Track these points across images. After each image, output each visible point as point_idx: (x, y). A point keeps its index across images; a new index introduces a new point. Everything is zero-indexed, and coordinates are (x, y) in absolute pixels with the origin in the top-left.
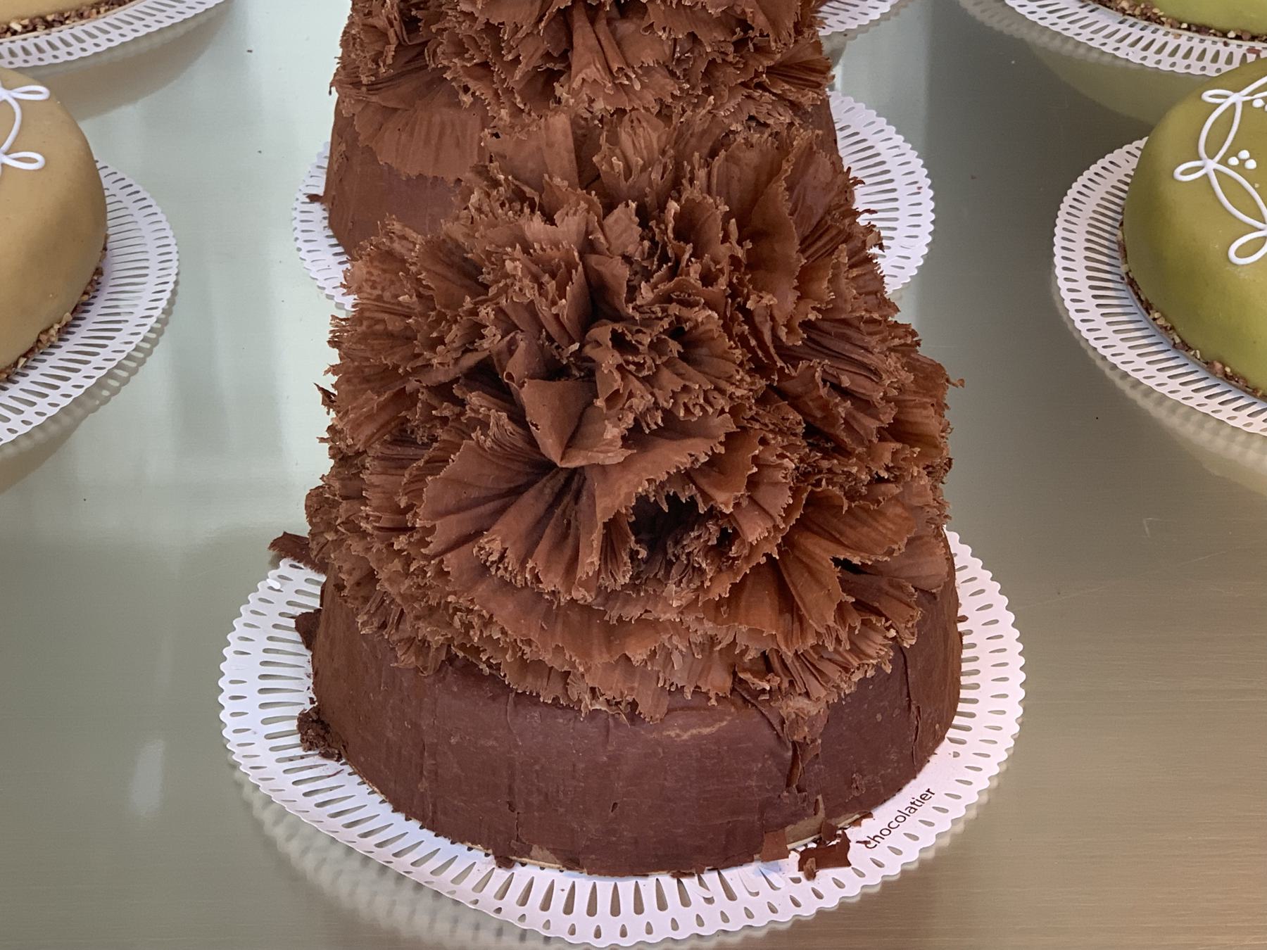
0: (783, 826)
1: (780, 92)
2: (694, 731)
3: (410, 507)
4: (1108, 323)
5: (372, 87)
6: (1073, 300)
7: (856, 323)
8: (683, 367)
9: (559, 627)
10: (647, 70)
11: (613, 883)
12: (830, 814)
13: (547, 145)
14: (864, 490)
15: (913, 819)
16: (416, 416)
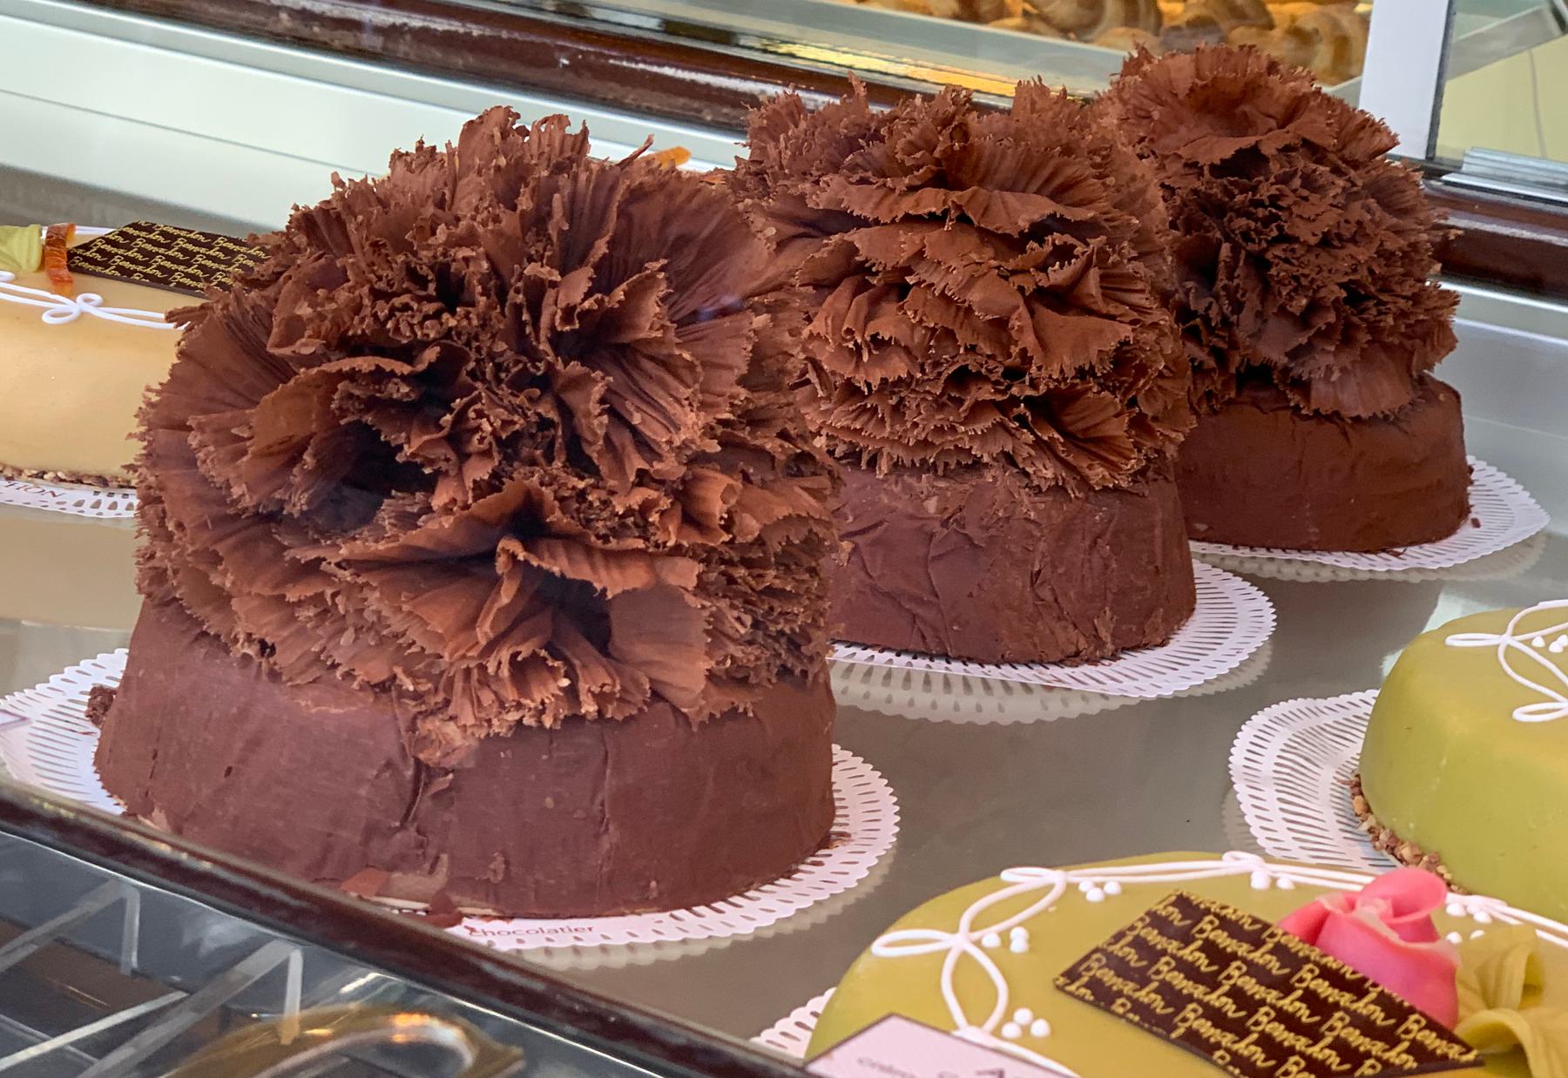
12: (454, 883)
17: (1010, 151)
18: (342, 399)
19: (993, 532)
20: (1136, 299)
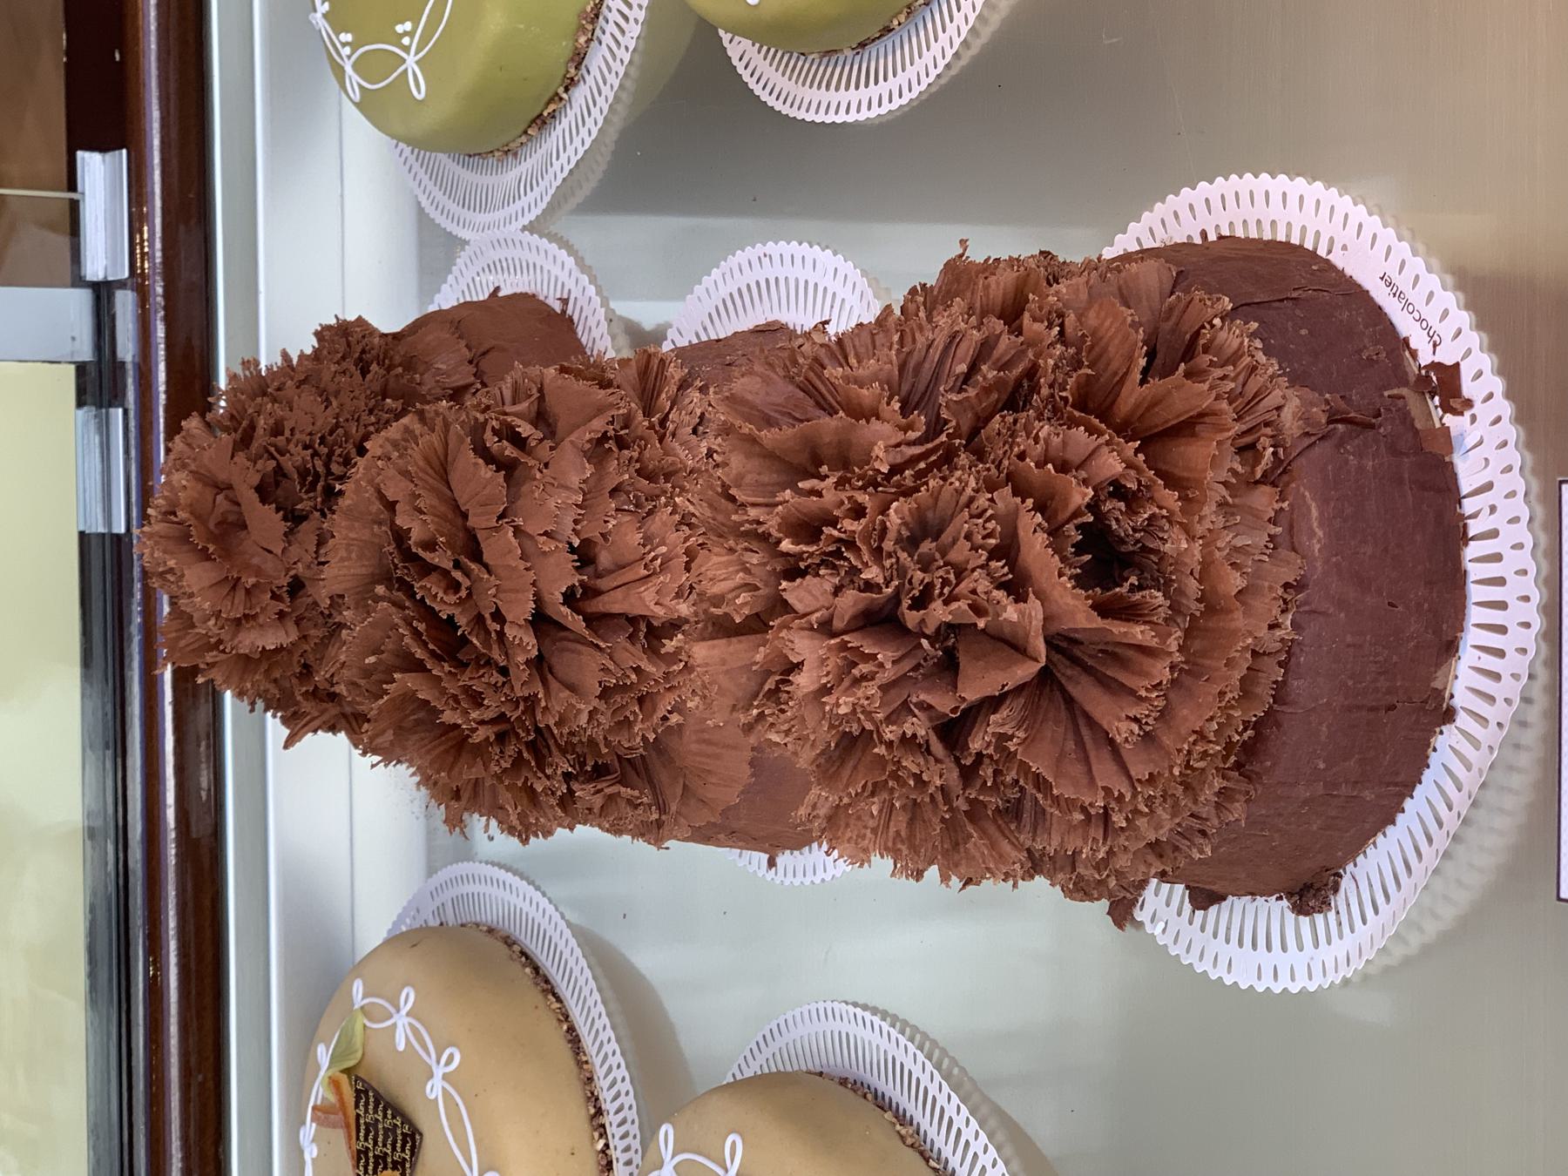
0: (1416, 432)
1: (669, 403)
2: (1315, 524)
3: (1084, 810)
4: (903, 70)
5: (662, 810)
6: (880, 105)
7: (903, 356)
8: (946, 537)
9: (1207, 662)
10: (647, 540)
11: (1474, 606)
12: (1404, 382)
13: (724, 665)
14: (1072, 351)
15: (1411, 295)
16: (993, 801)
17: (428, 502)
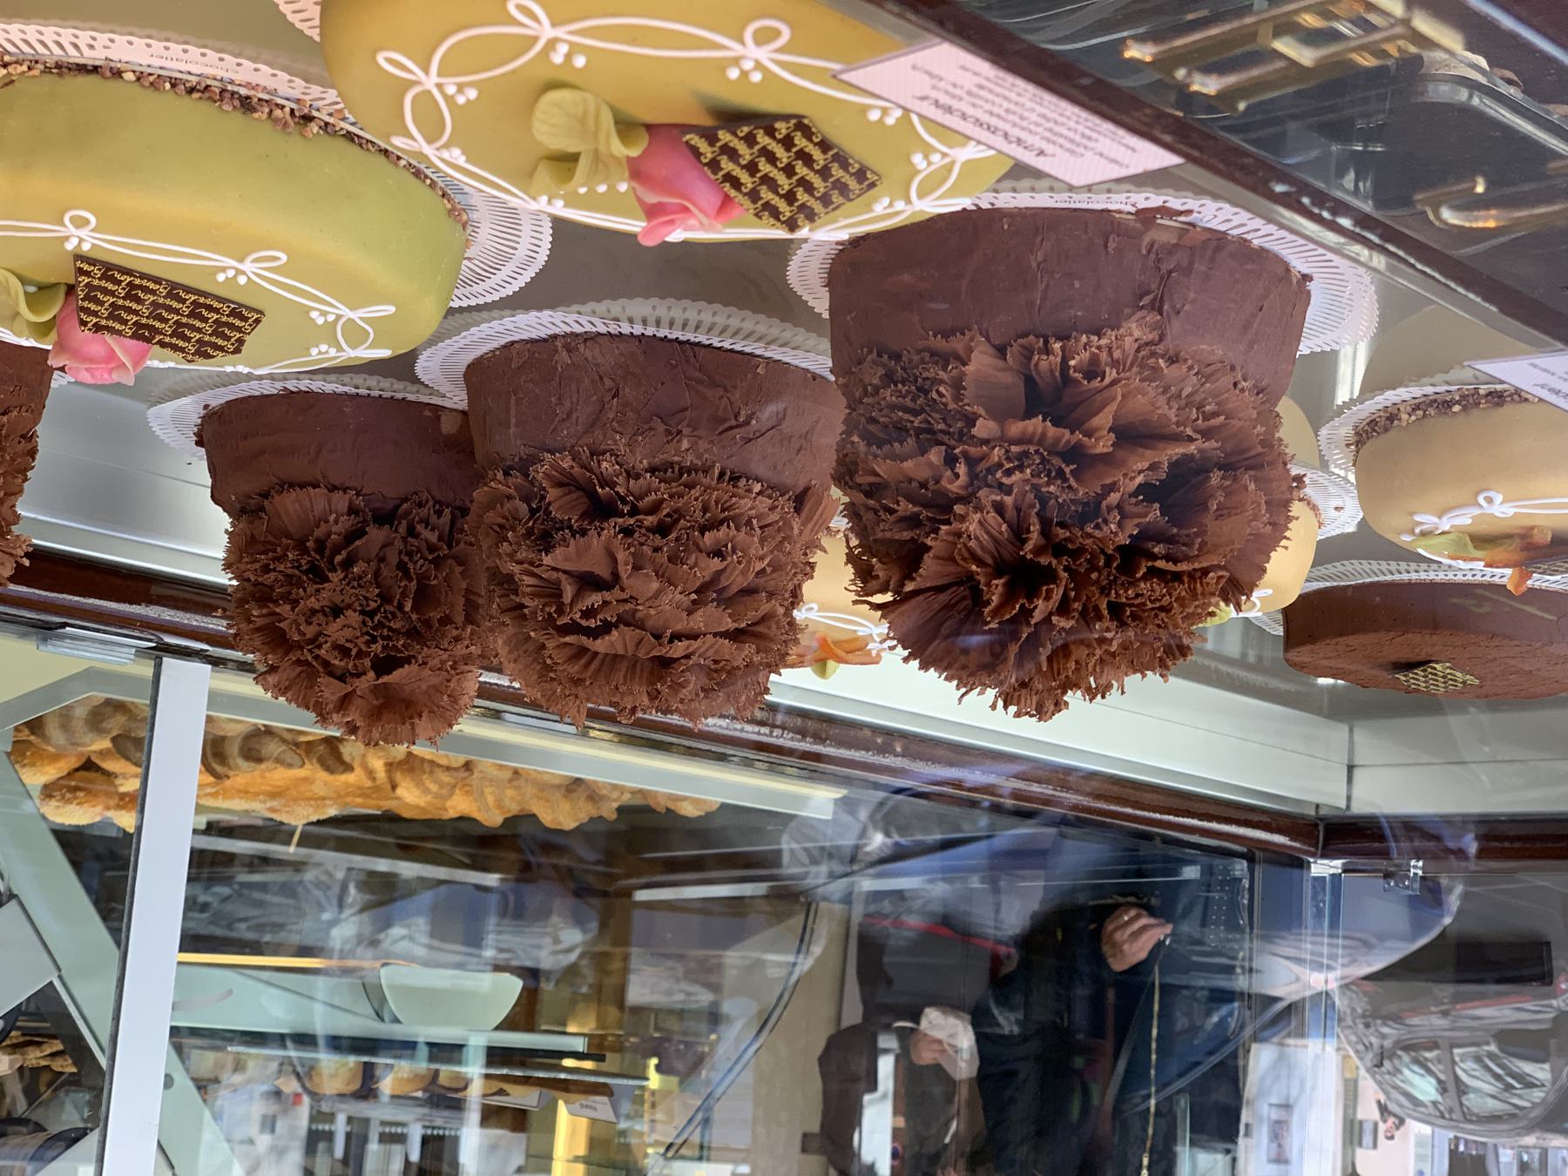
18: (1193, 544)
19: (646, 427)
20: (528, 580)
